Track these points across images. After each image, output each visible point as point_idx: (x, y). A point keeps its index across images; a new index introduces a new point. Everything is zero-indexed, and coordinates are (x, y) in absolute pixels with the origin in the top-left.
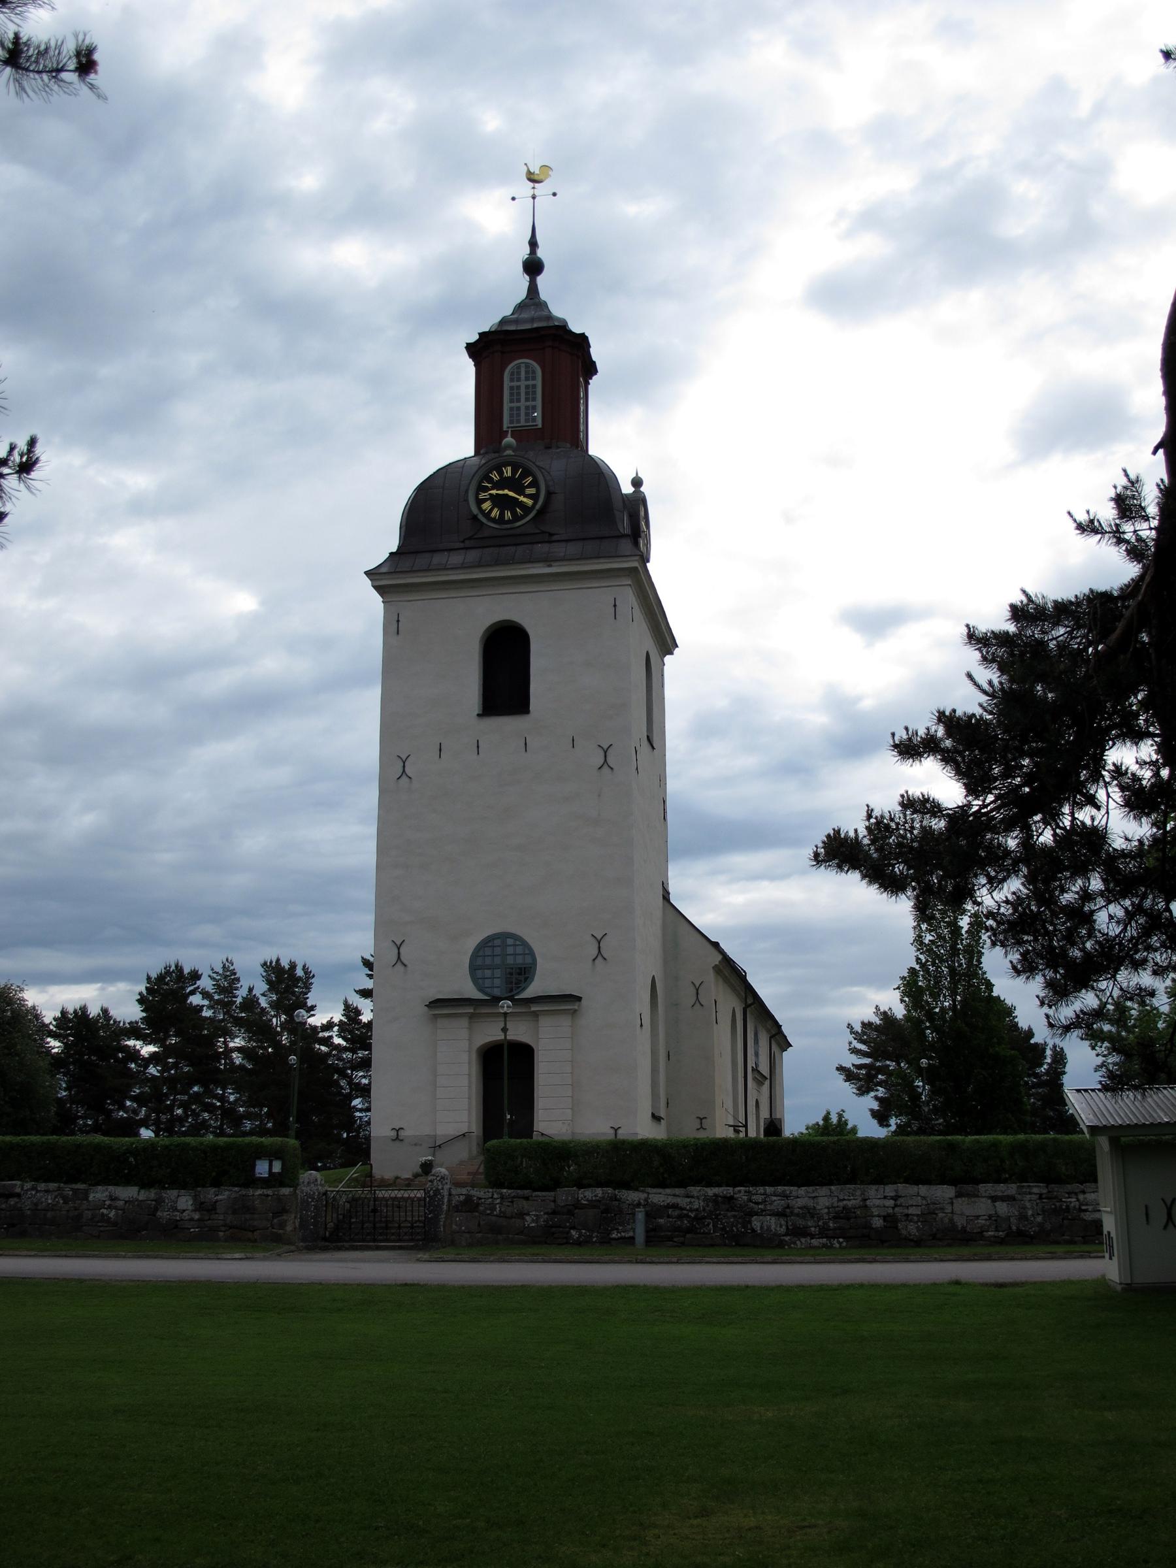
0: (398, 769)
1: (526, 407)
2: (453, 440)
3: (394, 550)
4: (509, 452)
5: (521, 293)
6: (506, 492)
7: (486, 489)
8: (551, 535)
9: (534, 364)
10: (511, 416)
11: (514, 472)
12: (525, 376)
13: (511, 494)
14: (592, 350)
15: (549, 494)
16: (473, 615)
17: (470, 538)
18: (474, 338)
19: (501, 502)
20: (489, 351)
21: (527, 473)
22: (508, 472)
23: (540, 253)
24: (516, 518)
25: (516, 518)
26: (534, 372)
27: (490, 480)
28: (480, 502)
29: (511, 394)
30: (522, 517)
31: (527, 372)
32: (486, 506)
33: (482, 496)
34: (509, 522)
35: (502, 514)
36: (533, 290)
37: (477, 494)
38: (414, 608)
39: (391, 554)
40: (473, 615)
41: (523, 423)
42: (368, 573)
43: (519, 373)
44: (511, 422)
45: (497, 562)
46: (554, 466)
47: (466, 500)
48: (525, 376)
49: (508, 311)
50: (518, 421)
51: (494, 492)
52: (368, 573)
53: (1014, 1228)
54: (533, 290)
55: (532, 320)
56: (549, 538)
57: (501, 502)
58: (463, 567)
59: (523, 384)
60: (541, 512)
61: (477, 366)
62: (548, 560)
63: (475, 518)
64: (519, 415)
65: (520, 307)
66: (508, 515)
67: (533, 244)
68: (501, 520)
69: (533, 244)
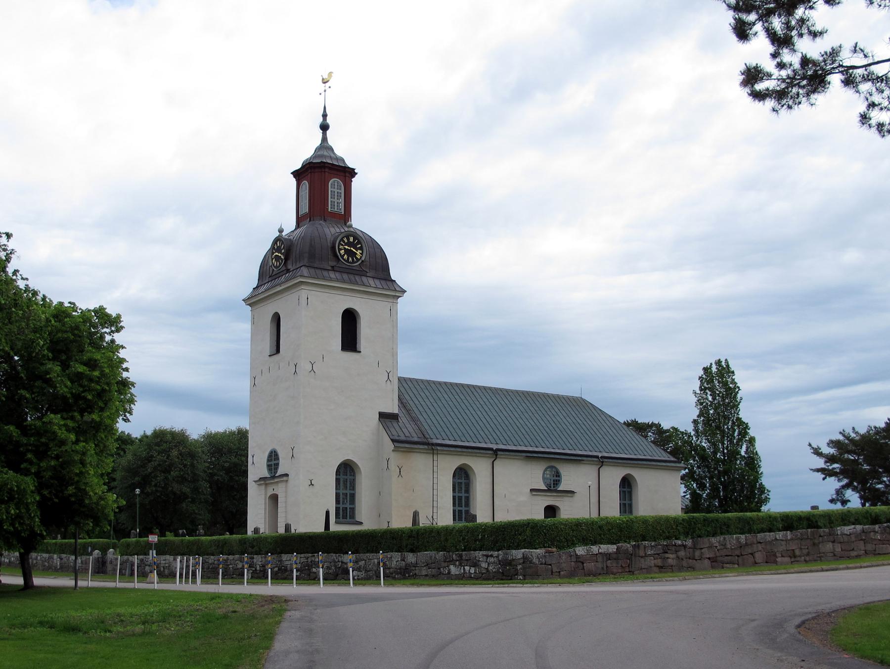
22: (351, 239)
23: (329, 120)
36: (324, 139)
54: (324, 139)
67: (325, 116)
69: (325, 116)
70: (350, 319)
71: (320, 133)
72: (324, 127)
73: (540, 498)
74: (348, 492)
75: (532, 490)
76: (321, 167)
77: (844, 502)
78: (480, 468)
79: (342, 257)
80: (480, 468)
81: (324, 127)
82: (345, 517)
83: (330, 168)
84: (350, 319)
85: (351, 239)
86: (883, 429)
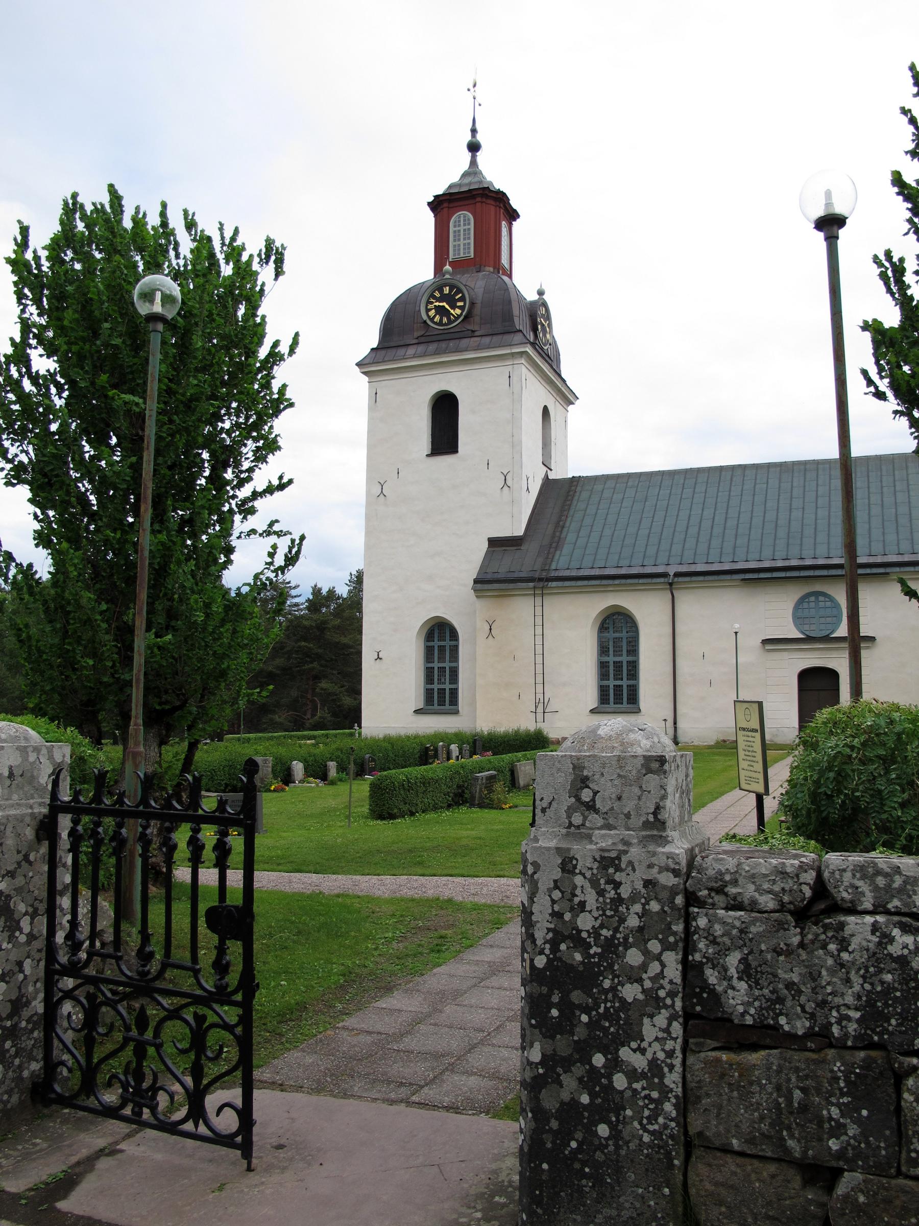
0: (379, 490)
1: (463, 244)
2: (420, 269)
3: (375, 346)
4: (447, 276)
5: (465, 165)
6: (444, 304)
7: (432, 303)
8: (473, 331)
9: (474, 212)
10: (454, 251)
11: (451, 290)
12: (463, 222)
13: (447, 307)
14: (511, 202)
15: (472, 304)
16: (418, 390)
17: (422, 336)
18: (431, 199)
19: (441, 311)
20: (442, 205)
21: (459, 291)
22: (446, 290)
23: (479, 137)
24: (450, 322)
25: (450, 322)
26: (469, 220)
27: (434, 297)
28: (428, 310)
29: (455, 236)
30: (446, 324)
31: (464, 220)
32: (432, 313)
33: (430, 306)
34: (446, 324)
35: (441, 320)
36: (473, 163)
37: (427, 306)
38: (392, 386)
39: (372, 349)
40: (418, 390)
41: (462, 255)
42: (357, 364)
43: (459, 221)
44: (454, 255)
45: (436, 353)
46: (476, 284)
47: (419, 311)
48: (463, 222)
49: (456, 178)
50: (459, 254)
51: (437, 304)
52: (357, 364)
53: (90, 850)
54: (473, 163)
55: (470, 184)
56: (472, 334)
57: (441, 311)
58: (414, 357)
59: (462, 228)
60: (466, 317)
61: (435, 216)
62: (478, 348)
63: (425, 322)
64: (459, 250)
65: (465, 175)
66: (445, 320)
67: (474, 131)
68: (440, 323)
69: (474, 131)
70: (445, 409)
71: (468, 156)
72: (474, 147)
73: (785, 655)
74: (611, 659)
75: (765, 642)
76: (495, 199)
77: (109, 1084)
78: (648, 610)
79: (432, 320)
80: (648, 610)
81: (474, 147)
82: (618, 700)
83: (450, 201)
84: (445, 409)
85: (446, 290)
86: (251, 270)
